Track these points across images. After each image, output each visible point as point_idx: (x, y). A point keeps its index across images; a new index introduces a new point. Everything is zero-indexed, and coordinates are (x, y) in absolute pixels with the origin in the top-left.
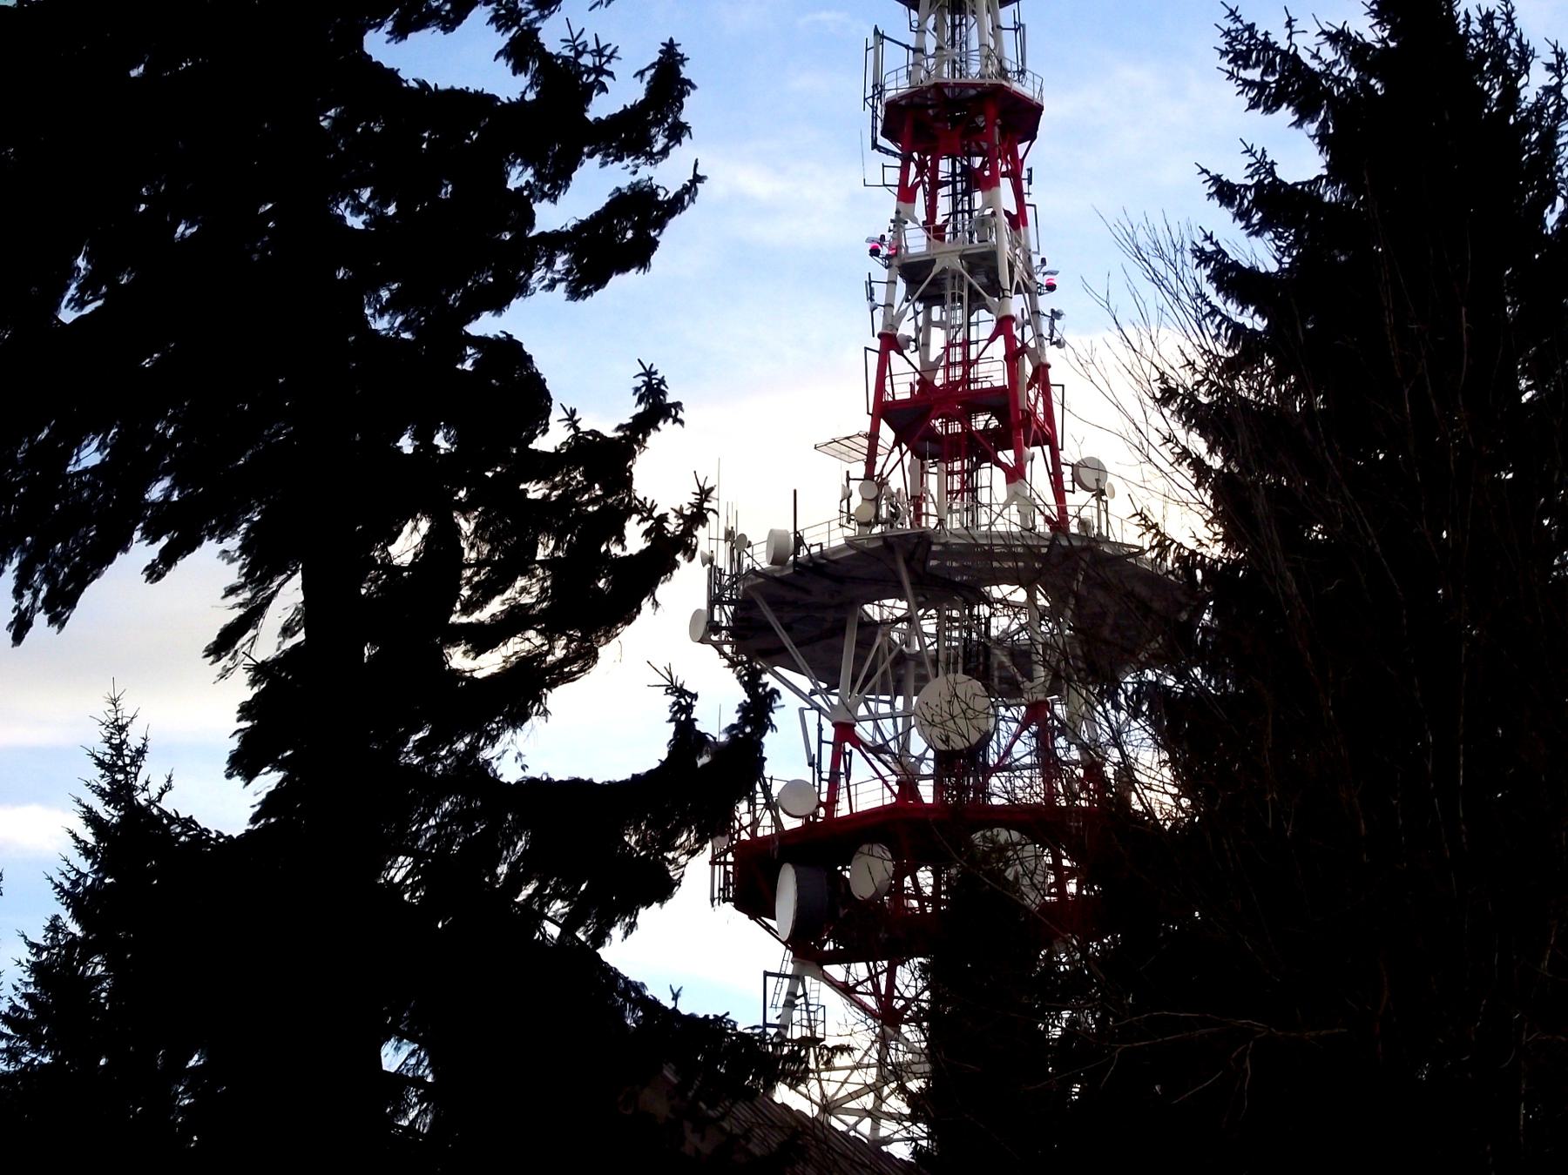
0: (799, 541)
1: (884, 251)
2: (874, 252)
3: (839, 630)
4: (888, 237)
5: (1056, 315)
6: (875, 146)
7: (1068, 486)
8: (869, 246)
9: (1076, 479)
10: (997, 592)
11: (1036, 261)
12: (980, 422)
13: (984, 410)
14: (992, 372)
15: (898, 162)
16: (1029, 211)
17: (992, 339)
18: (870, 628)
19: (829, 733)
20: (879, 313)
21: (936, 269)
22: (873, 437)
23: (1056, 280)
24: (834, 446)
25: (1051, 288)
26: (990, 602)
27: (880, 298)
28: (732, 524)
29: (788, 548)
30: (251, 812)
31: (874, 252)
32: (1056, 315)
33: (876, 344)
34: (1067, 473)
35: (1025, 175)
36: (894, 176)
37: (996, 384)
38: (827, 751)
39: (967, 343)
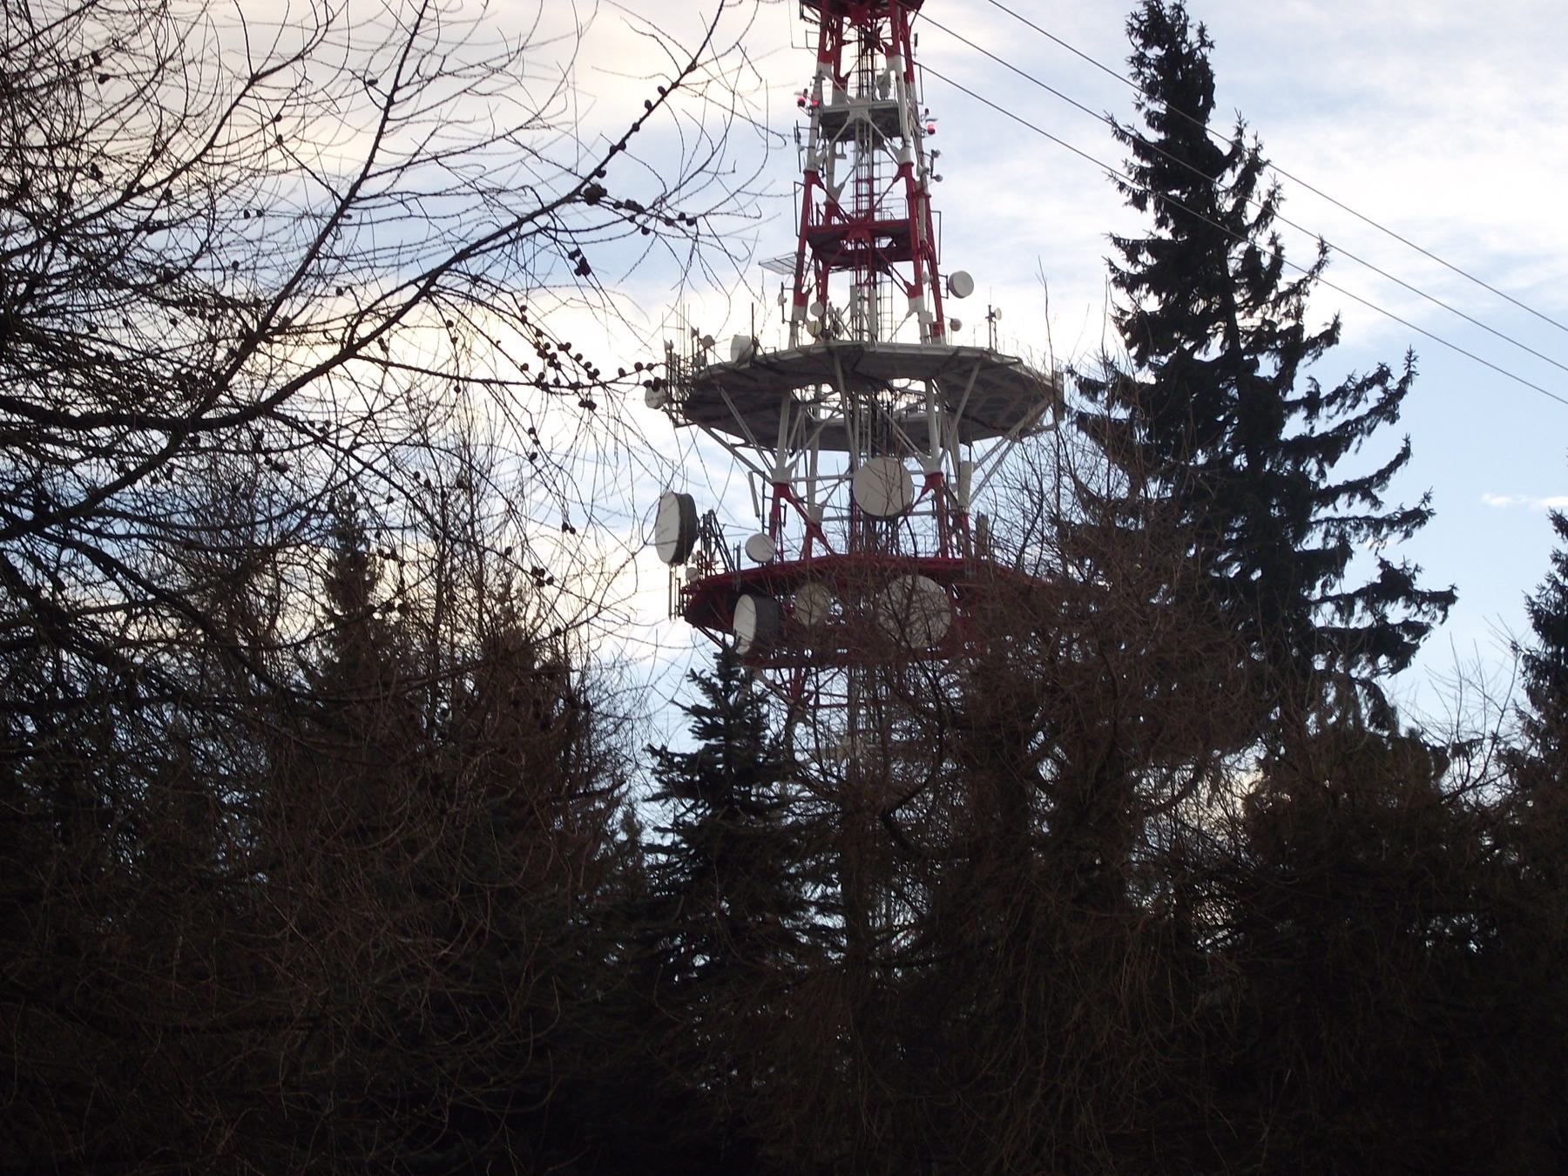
0: (756, 343)
1: (808, 103)
2: (801, 103)
3: (776, 406)
4: (810, 91)
5: (935, 154)
6: (802, 16)
7: (943, 292)
8: (796, 99)
9: (949, 287)
10: (898, 383)
11: (921, 111)
12: (884, 243)
13: (886, 235)
14: (895, 207)
15: (817, 29)
16: (916, 68)
17: (896, 180)
18: (796, 403)
19: (770, 490)
20: (804, 154)
21: (849, 120)
22: (801, 254)
23: (935, 126)
24: (774, 265)
25: (932, 132)
26: (892, 390)
27: (805, 142)
28: (590, 276)
29: (747, 350)
30: (1418, 652)
31: (801, 103)
32: (935, 154)
33: (802, 178)
34: (943, 286)
35: (912, 39)
36: (815, 41)
37: (898, 217)
38: (769, 504)
39: (870, 180)
